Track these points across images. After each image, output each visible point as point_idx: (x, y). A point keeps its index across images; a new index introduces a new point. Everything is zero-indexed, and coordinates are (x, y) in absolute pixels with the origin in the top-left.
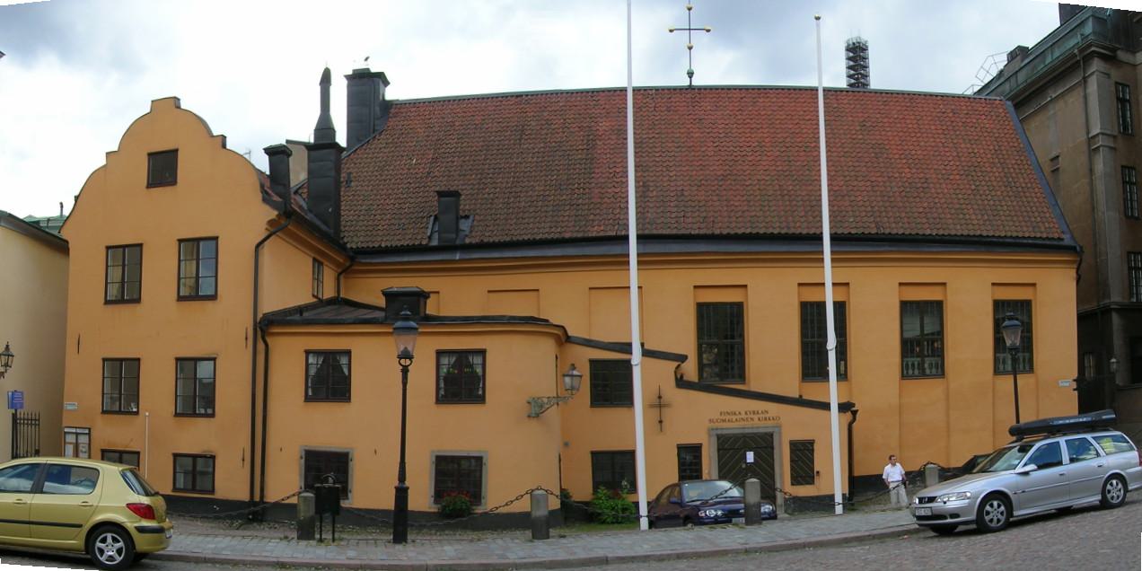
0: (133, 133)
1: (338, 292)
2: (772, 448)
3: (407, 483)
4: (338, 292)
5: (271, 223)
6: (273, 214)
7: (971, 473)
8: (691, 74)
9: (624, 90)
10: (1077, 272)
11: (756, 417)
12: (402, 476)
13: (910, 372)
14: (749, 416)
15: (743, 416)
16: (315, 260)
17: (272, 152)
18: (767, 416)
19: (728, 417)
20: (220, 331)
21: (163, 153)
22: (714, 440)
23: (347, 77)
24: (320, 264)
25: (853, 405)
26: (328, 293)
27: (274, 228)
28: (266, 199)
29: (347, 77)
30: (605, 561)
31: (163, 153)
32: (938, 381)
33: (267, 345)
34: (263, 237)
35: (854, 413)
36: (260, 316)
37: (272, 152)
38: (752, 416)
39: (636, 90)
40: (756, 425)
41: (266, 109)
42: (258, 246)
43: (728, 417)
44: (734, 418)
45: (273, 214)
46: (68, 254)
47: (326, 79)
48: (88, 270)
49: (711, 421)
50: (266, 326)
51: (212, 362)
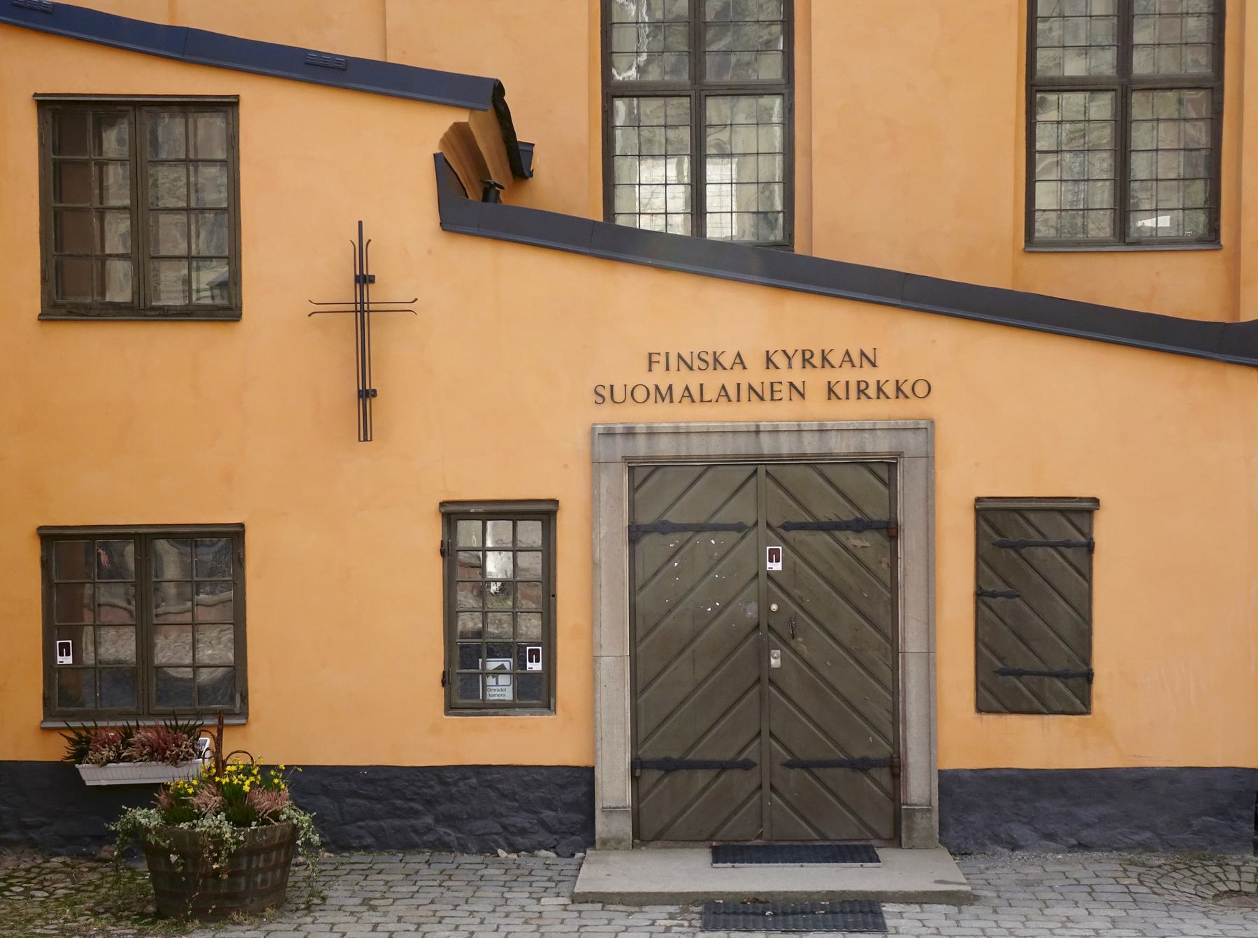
2: (890, 530)
11: (815, 380)
14: (785, 375)
15: (757, 375)
18: (870, 375)
19: (680, 378)
22: (617, 483)
38: (797, 375)
40: (809, 417)
43: (680, 378)
44: (713, 381)
49: (604, 395)
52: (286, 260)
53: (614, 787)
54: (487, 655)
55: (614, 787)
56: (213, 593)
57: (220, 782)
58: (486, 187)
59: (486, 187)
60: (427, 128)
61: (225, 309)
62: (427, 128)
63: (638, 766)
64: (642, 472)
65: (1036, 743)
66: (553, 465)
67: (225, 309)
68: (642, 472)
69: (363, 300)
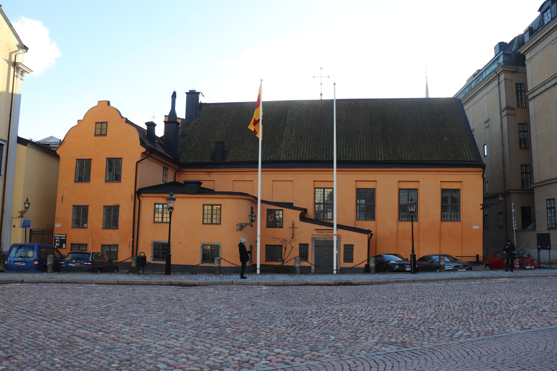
0: (91, 112)
1: (175, 179)
3: (415, 253)
4: (175, 179)
5: (143, 153)
6: (144, 150)
7: (250, 252)
8: (321, 95)
9: (333, 100)
10: (483, 176)
12: (413, 252)
13: (445, 218)
16: (164, 168)
17: (147, 124)
20: (122, 194)
21: (102, 120)
22: (314, 242)
23: (187, 93)
24: (167, 169)
25: (371, 231)
26: (170, 179)
27: (146, 156)
28: (142, 143)
29: (187, 93)
30: (350, 284)
31: (102, 120)
32: (116, 230)
33: (140, 200)
34: (140, 159)
35: (372, 235)
36: (137, 189)
37: (147, 124)
39: (337, 100)
41: (149, 107)
42: (138, 162)
45: (144, 150)
46: (59, 159)
47: (174, 95)
48: (67, 168)
49: (313, 235)
50: (139, 193)
51: (317, 190)
52: (287, 224)
53: (313, 268)
54: (304, 256)
55: (313, 268)
56: (489, 330)
57: (531, 265)
58: (304, 217)
59: (304, 217)
60: (299, 212)
61: (282, 227)
62: (299, 212)
63: (261, 265)
64: (316, 241)
65: (349, 265)
66: (308, 241)
67: (282, 227)
68: (316, 241)
69: (293, 227)
